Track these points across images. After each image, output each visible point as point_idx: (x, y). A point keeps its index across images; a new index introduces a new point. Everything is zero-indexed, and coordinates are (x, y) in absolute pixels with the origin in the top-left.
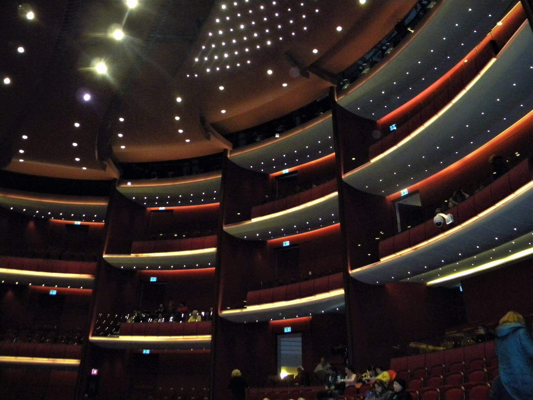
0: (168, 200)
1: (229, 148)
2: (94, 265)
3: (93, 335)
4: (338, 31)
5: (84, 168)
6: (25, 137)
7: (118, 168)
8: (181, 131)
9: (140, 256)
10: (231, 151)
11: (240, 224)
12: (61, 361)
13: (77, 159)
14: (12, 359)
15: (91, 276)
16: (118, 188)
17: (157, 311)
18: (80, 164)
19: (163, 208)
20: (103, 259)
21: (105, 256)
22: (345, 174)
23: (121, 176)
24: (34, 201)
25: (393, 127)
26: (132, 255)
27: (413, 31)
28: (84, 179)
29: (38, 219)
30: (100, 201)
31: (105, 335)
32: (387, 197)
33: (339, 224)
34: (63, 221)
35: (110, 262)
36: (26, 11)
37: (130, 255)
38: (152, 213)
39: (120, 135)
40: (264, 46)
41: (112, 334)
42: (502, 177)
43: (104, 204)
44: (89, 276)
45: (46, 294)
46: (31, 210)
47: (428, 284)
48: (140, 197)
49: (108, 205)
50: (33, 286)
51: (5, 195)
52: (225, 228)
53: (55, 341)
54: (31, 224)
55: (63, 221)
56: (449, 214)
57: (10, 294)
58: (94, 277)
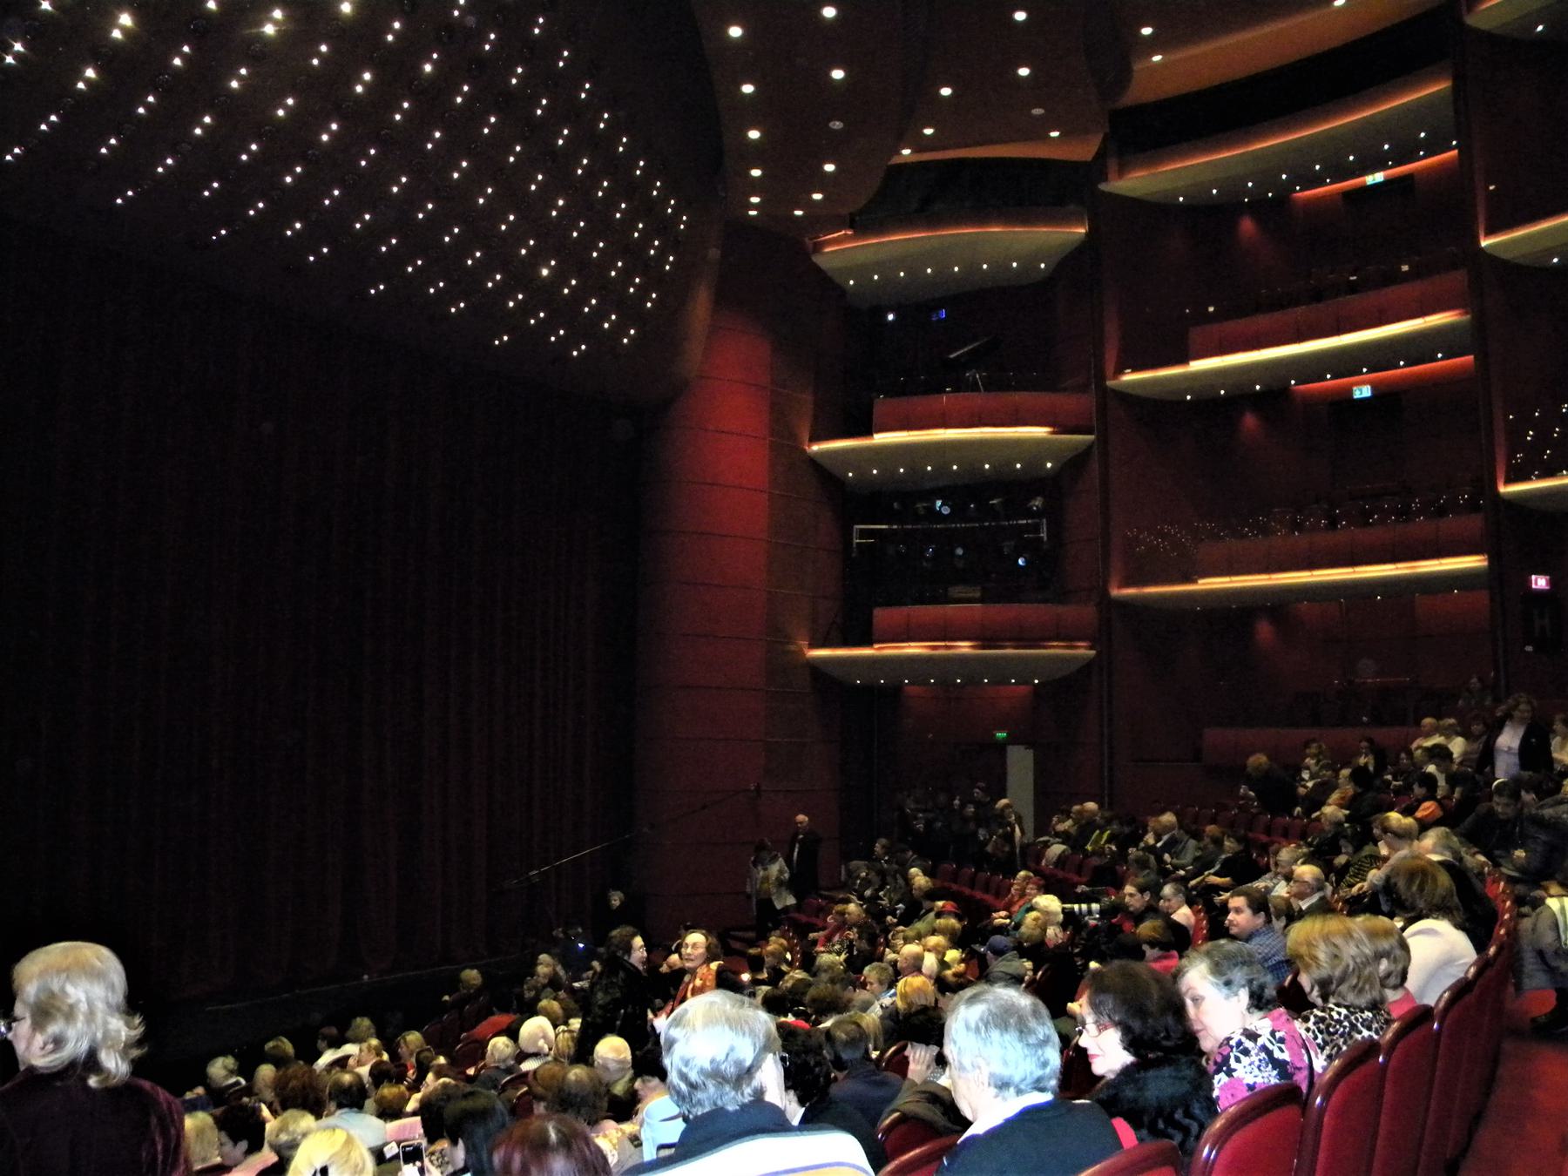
2: (1459, 278)
6: (946, 92)
16: (1471, 20)
20: (1482, 250)
21: (1485, 243)
24: (1278, 144)
29: (1259, 208)
36: (116, 12)
42: (1243, 320)
43: (1437, 88)
44: (1456, 315)
45: (1344, 400)
46: (1232, 187)
50: (1302, 387)
51: (1153, 171)
53: (1405, 514)
54: (1247, 225)
57: (1250, 421)
58: (1467, 313)
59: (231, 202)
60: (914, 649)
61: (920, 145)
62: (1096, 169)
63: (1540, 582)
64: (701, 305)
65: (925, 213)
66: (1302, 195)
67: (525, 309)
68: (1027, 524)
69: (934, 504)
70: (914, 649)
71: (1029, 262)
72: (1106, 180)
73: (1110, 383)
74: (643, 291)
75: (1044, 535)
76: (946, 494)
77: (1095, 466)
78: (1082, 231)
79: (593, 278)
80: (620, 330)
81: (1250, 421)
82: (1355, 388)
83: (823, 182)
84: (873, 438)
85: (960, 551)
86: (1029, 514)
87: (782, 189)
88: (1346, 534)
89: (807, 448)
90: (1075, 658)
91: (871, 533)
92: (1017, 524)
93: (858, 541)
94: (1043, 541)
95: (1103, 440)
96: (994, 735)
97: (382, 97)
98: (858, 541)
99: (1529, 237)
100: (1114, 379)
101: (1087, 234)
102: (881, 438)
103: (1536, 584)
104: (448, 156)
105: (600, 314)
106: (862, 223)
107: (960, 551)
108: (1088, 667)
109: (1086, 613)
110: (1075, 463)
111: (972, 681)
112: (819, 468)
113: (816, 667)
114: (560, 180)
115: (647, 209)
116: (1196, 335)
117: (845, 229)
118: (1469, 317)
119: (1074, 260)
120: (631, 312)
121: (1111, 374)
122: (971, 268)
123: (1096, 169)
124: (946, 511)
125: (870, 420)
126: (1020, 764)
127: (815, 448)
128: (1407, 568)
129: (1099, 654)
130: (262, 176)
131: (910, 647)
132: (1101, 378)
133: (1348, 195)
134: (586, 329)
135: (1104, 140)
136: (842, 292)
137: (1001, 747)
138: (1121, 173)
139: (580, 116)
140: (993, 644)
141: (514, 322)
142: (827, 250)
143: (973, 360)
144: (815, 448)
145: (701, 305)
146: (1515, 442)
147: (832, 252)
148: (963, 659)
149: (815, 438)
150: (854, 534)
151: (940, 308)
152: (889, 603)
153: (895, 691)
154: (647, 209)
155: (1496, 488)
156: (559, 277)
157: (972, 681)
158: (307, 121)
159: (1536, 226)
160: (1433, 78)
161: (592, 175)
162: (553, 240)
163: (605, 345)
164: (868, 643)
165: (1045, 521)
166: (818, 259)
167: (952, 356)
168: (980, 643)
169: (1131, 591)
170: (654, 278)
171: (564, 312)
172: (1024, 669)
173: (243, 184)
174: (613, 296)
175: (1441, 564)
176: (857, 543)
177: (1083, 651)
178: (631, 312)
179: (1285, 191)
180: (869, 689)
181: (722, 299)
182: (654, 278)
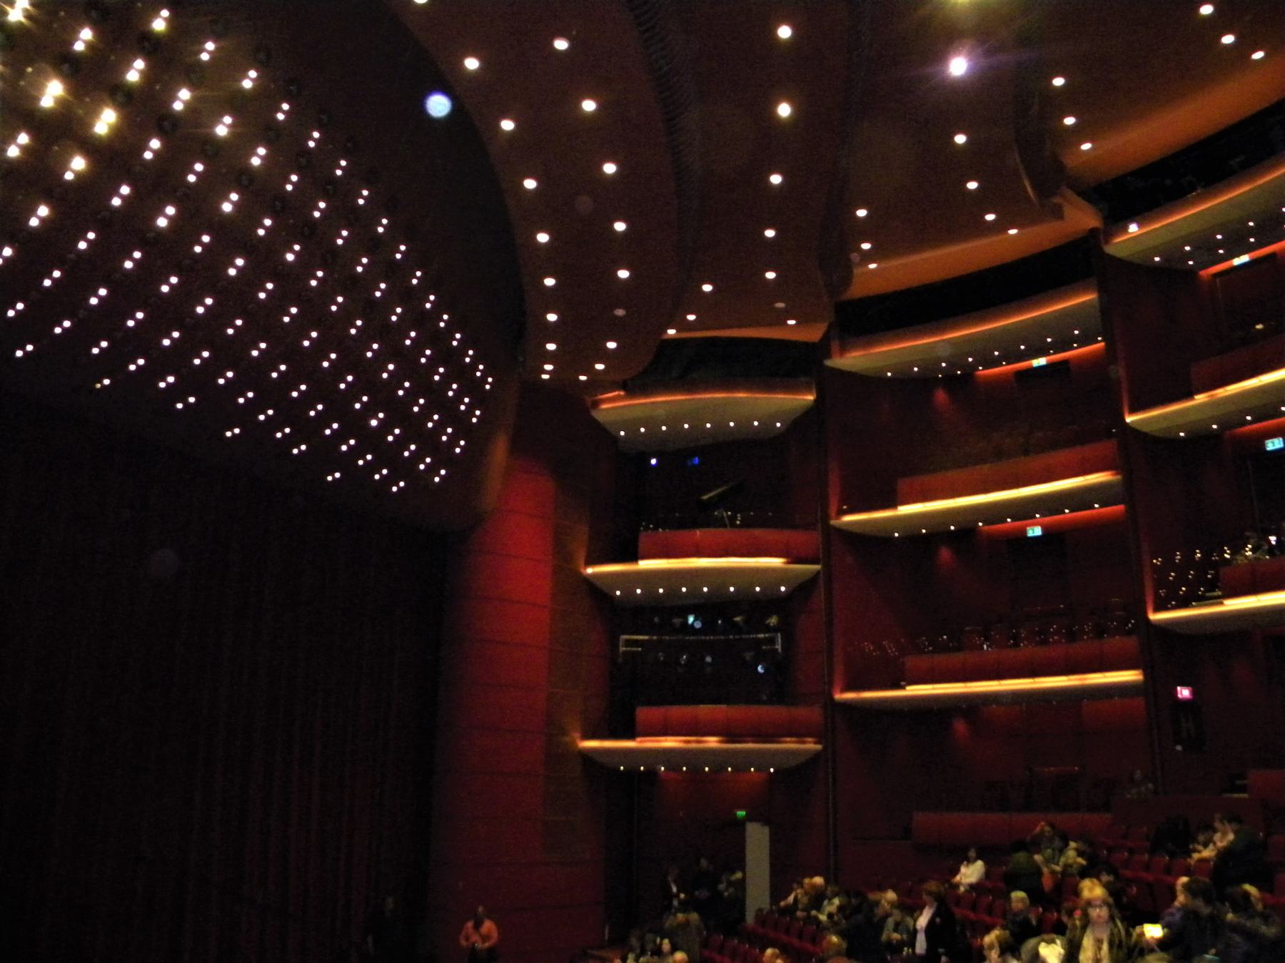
0: (1251, 232)
3: (1158, 609)
4: (466, 69)
5: (1013, 232)
7: (1089, 201)
8: (1228, 39)
9: (1219, 396)
12: (1096, 678)
13: (990, 217)
14: (992, 686)
15: (1112, 475)
18: (1000, 227)
19: (1244, 259)
20: (1127, 424)
26: (1197, 397)
28: (987, 266)
31: (1184, 604)
34: (1005, 368)
35: (1146, 429)
37: (1193, 399)
38: (1218, 280)
39: (1070, 121)
40: (356, 177)
41: (1202, 600)
43: (1087, 298)
44: (1108, 475)
45: (1020, 539)
46: (930, 366)
47: (772, 624)
48: (1172, 253)
50: (986, 528)
53: (1072, 637)
55: (1005, 368)
57: (945, 554)
58: (1117, 474)
59: (113, 362)
60: (670, 743)
61: (683, 326)
62: (821, 349)
63: (1184, 693)
64: (499, 451)
65: (685, 382)
66: (982, 372)
67: (356, 452)
68: (765, 637)
69: (687, 620)
70: (670, 743)
71: (767, 423)
72: (829, 356)
73: (833, 522)
74: (453, 440)
75: (779, 647)
76: (697, 610)
77: (820, 595)
78: (811, 398)
79: (414, 429)
80: (433, 469)
81: (945, 554)
82: (1028, 528)
83: (605, 356)
84: (638, 564)
85: (709, 659)
86: (768, 629)
87: (569, 360)
88: (1027, 650)
90: (806, 751)
91: (636, 643)
92: (756, 637)
93: (624, 649)
94: (778, 653)
95: (827, 566)
96: (735, 814)
97: (250, 279)
98: (624, 649)
99: (1164, 417)
101: (815, 401)
102: (645, 565)
103: (1181, 694)
104: (300, 327)
105: (417, 457)
106: (633, 387)
107: (709, 659)
108: (816, 757)
109: (811, 713)
110: (804, 588)
111: (718, 769)
112: (595, 589)
113: (587, 756)
114: (393, 350)
115: (460, 373)
116: (903, 485)
117: (619, 390)
119: (802, 423)
120: (442, 455)
121: (834, 515)
122: (720, 426)
123: (821, 349)
124: (698, 625)
125: (636, 547)
126: (758, 839)
127: (590, 570)
128: (1076, 680)
129: (825, 748)
130: (143, 340)
131: (666, 741)
132: (826, 518)
133: (1021, 374)
134: (403, 469)
135: (830, 326)
136: (616, 439)
137: (741, 824)
138: (843, 350)
139: (410, 298)
140: (738, 739)
141: (346, 462)
142: (604, 406)
143: (720, 501)
144: (590, 570)
145: (499, 451)
146: (1160, 582)
147: (608, 409)
148: (713, 752)
149: (591, 562)
150: (621, 643)
151: (694, 456)
152: (650, 703)
153: (652, 774)
154: (460, 373)
156: (385, 427)
157: (718, 769)
158: (187, 295)
160: (1085, 290)
161: (418, 346)
162: (383, 397)
163: (418, 482)
164: (631, 736)
165: (779, 635)
166: (596, 414)
167: (705, 497)
169: (850, 696)
170: (463, 428)
171: (388, 455)
172: (760, 760)
173: (126, 345)
174: (429, 443)
175: (1105, 677)
176: (625, 653)
177: (811, 746)
178: (442, 455)
179: (970, 371)
180: (632, 773)
181: (516, 447)
182: (463, 428)
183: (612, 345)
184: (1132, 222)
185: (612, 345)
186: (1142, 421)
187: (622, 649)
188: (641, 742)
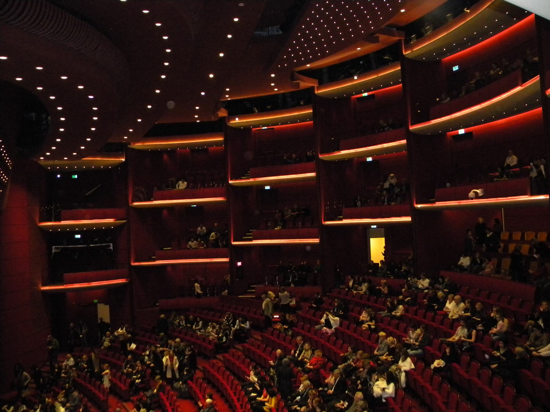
1: (316, 86)
10: (317, 87)
11: (332, 154)
17: (343, 354)
22: (412, 126)
23: (228, 114)
25: (456, 68)
27: (469, 11)
30: (216, 137)
32: (442, 60)
33: (405, 141)
35: (233, 185)
49: (224, 140)
52: (320, 156)
56: (481, 189)
73: (130, 205)
75: (112, 248)
86: (231, 323)
89: (38, 224)
91: (57, 248)
100: (131, 204)
102: (63, 223)
118: (226, 200)
131: (76, 285)
155: (231, 243)
159: (348, 56)
168: (116, 219)
183: (58, 140)
184: (237, 117)
185: (58, 140)
186: (233, 183)
187: (53, 251)
188: (65, 286)
